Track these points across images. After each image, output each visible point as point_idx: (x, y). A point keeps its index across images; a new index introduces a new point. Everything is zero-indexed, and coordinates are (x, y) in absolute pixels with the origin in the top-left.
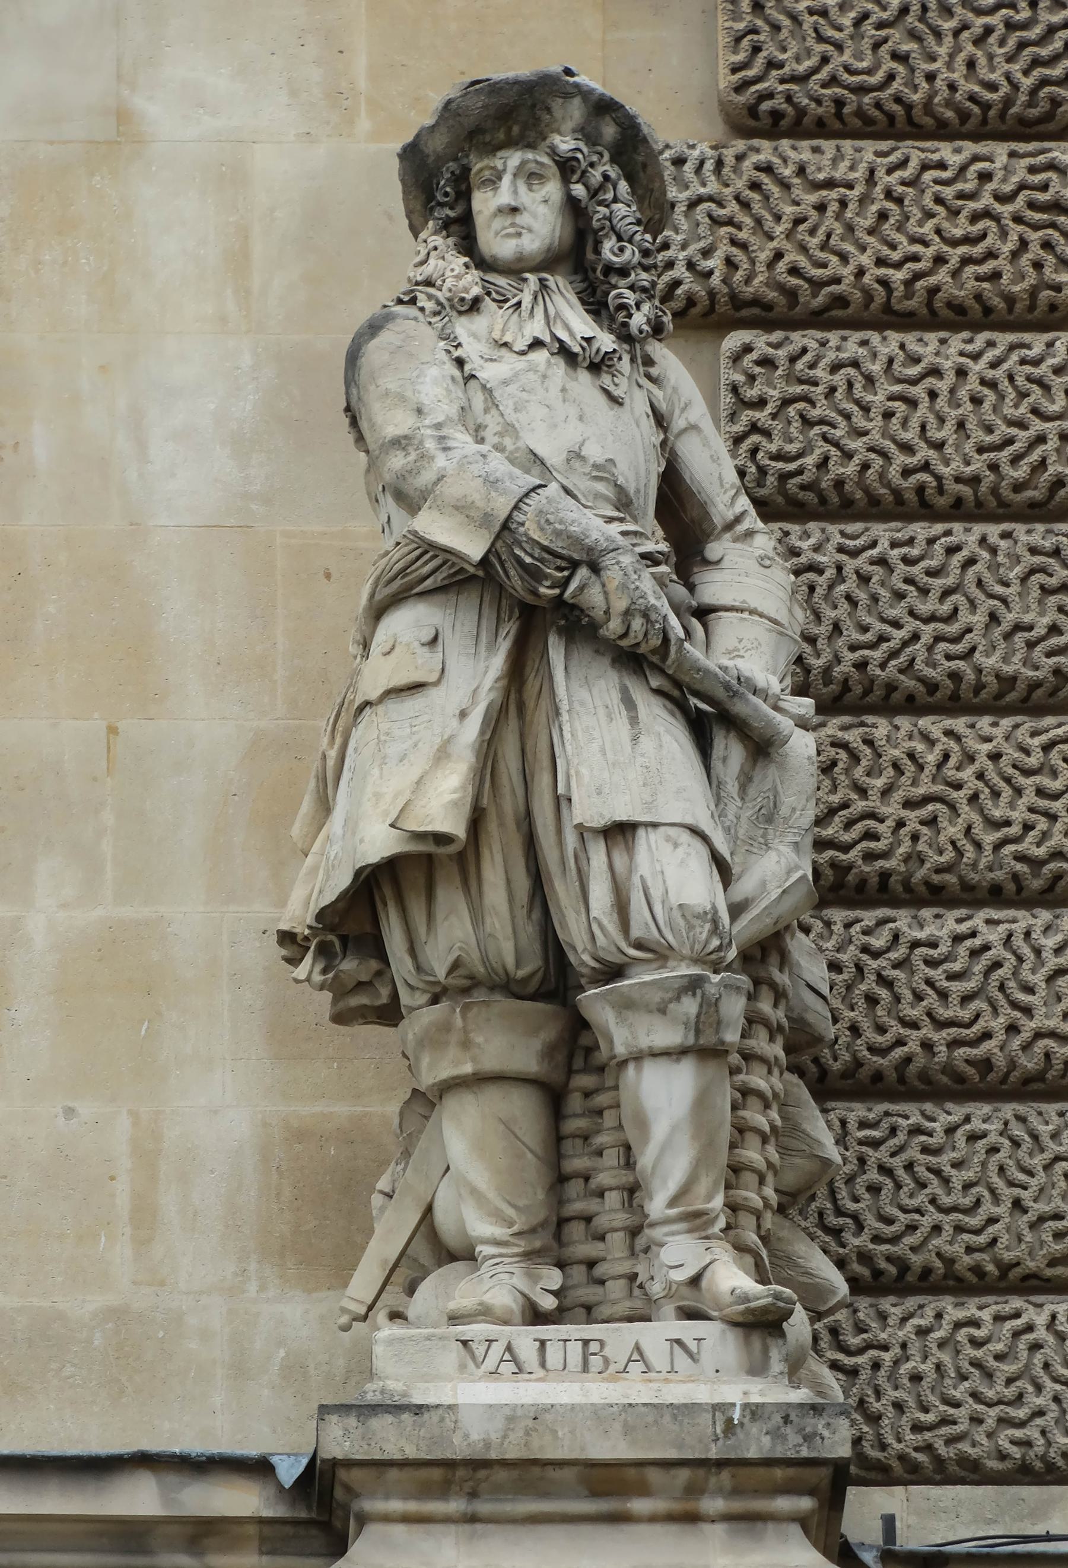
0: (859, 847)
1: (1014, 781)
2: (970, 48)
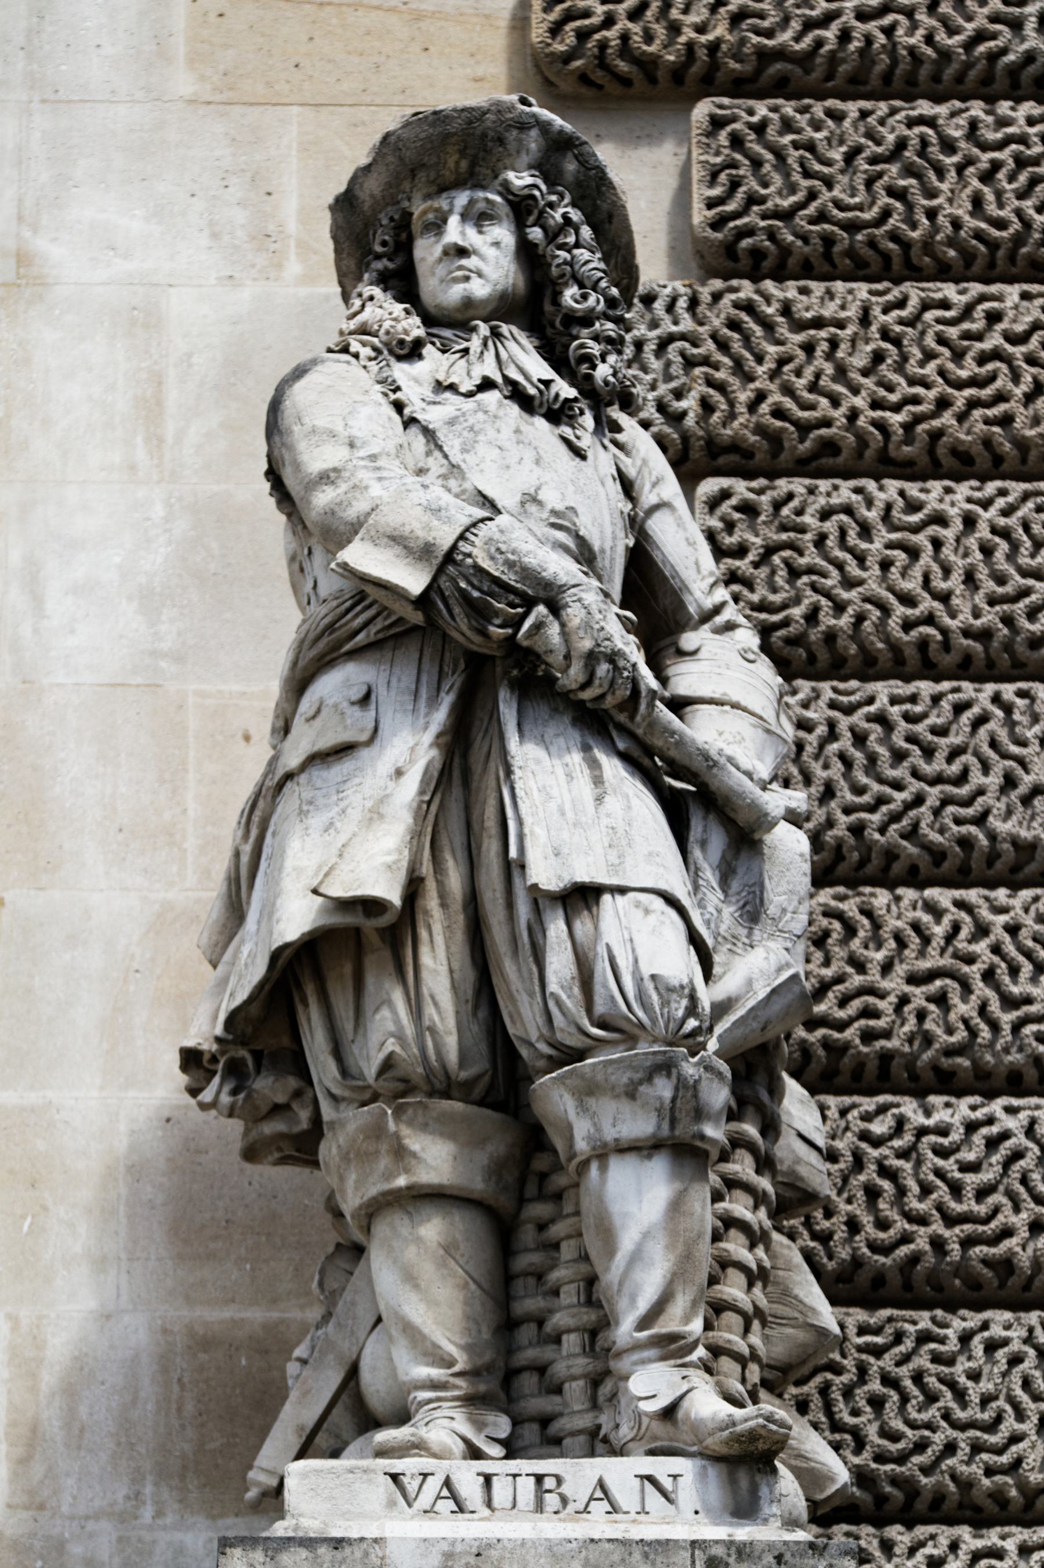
0: (856, 1025)
1: (1035, 955)
2: (975, 183)
